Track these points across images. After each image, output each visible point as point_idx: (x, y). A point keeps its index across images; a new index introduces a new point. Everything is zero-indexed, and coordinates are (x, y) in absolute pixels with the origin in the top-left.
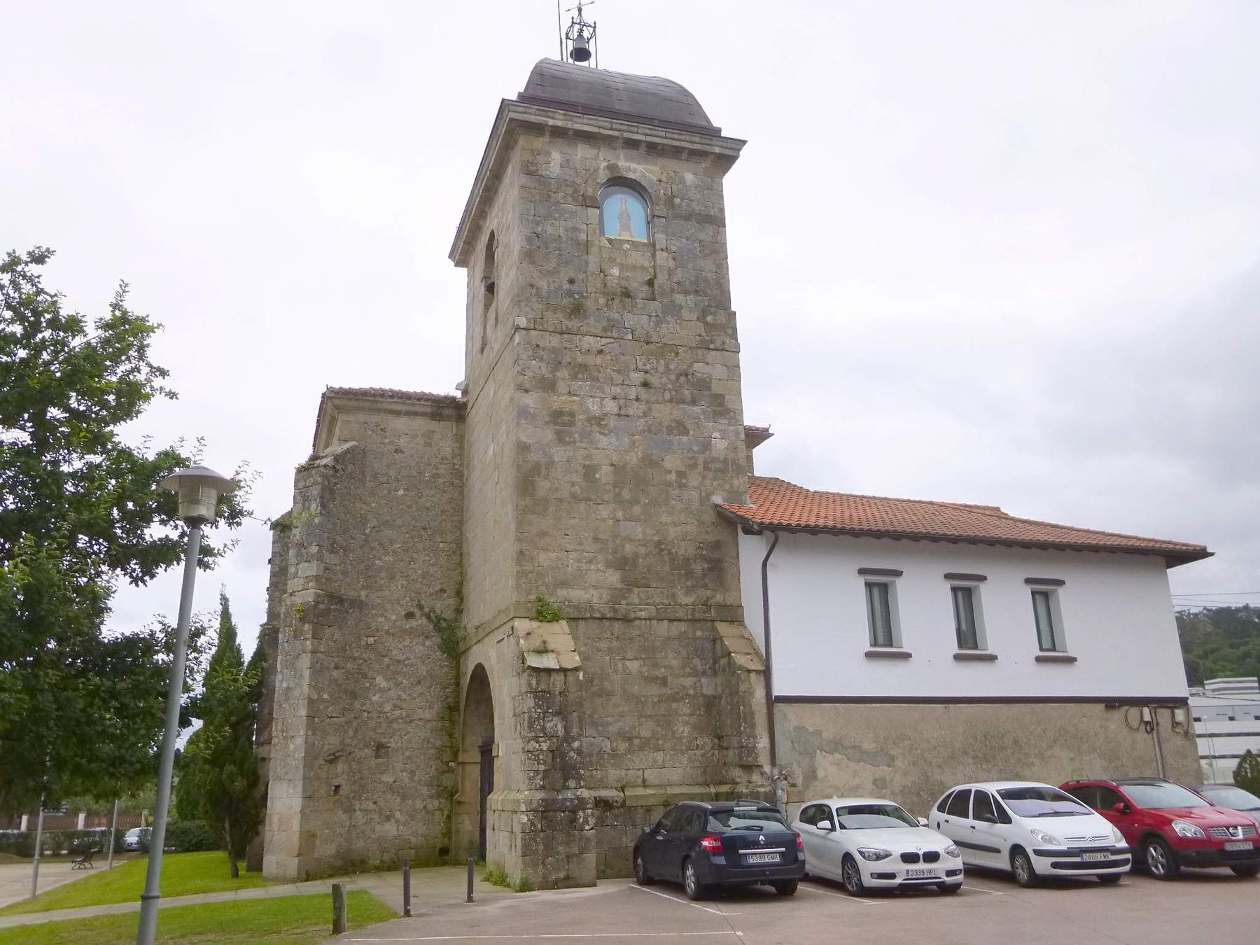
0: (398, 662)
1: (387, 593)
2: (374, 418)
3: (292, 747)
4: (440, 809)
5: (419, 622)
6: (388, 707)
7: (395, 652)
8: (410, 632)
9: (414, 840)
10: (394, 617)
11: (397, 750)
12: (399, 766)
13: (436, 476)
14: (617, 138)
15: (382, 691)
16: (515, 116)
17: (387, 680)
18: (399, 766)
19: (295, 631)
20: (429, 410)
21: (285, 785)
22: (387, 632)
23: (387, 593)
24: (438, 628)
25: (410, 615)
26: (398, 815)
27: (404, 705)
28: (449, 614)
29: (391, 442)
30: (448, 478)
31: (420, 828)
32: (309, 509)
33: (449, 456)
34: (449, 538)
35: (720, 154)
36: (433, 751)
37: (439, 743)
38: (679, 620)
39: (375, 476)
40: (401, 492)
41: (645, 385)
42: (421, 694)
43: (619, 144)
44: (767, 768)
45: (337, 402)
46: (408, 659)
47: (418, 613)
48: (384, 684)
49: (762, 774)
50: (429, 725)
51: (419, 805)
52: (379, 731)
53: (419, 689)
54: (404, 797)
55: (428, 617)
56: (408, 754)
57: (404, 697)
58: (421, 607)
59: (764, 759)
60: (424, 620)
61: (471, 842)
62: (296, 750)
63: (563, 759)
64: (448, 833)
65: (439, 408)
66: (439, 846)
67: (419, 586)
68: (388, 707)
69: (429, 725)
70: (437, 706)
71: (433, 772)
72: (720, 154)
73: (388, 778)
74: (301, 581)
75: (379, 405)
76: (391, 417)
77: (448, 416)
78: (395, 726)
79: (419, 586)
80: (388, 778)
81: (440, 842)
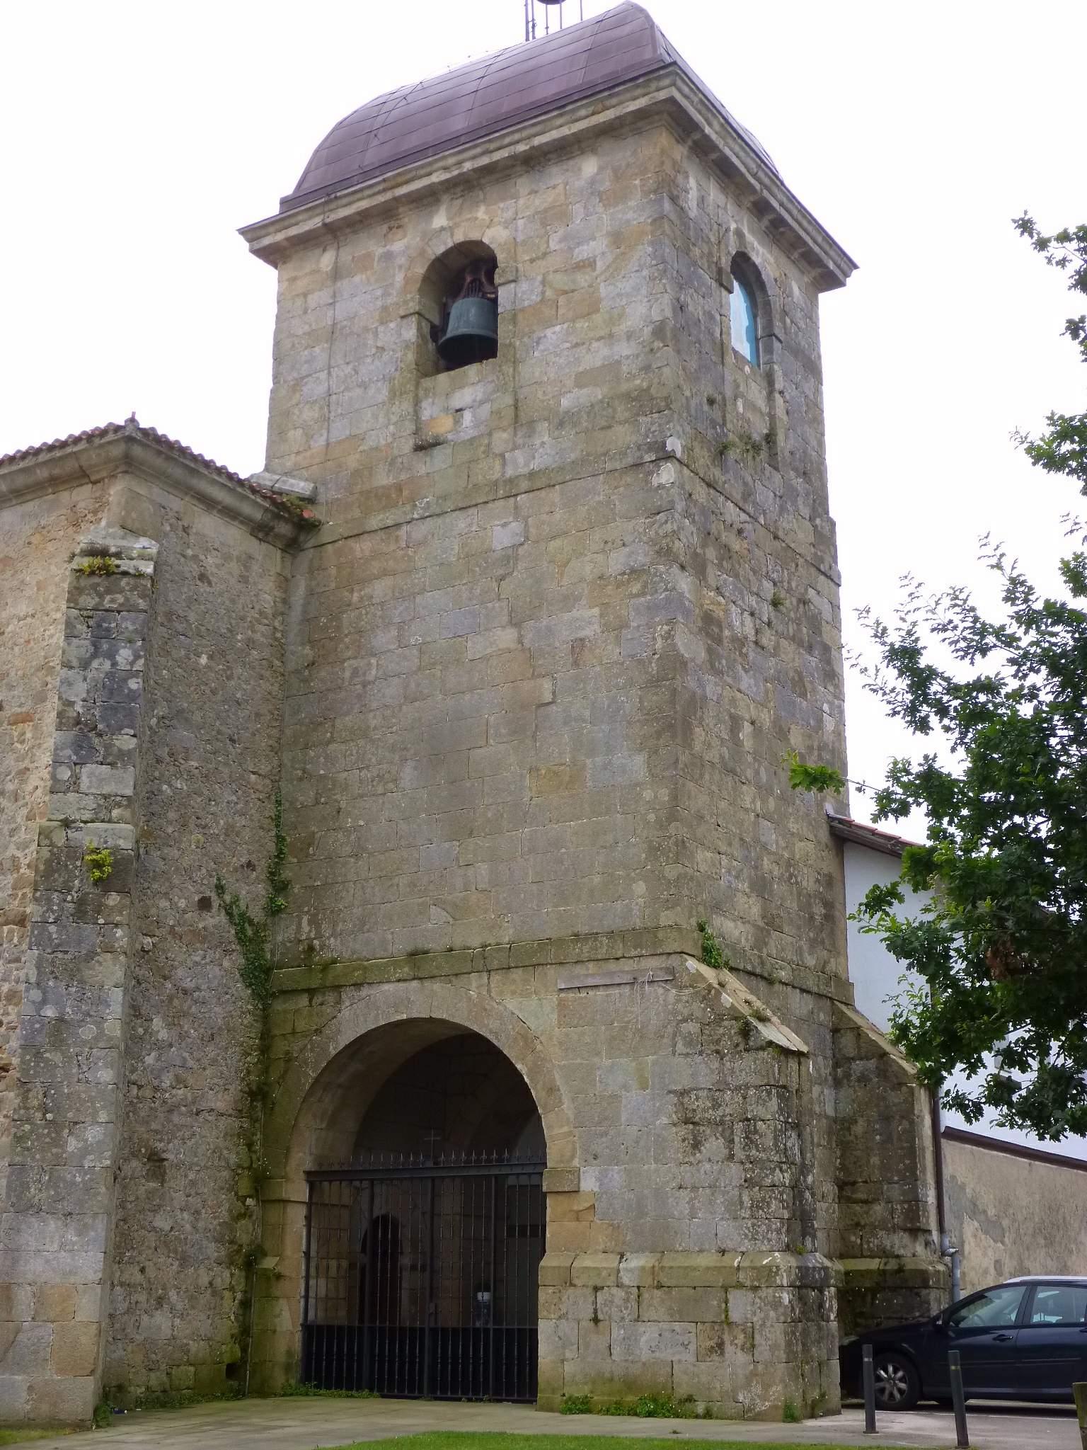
0: (185, 992)
1: (176, 853)
2: (176, 503)
3: (72, 1145)
4: (232, 1289)
5: (215, 919)
6: (167, 1081)
7: (180, 972)
8: (201, 936)
9: (194, 1347)
10: (182, 904)
11: (178, 1167)
12: (179, 1198)
13: (250, 643)
14: (754, 191)
15: (161, 1047)
16: (678, 96)
17: (170, 1025)
18: (179, 1198)
19: (81, 903)
20: (258, 515)
21: (52, 1225)
22: (172, 930)
23: (176, 853)
24: (241, 938)
25: (204, 904)
26: (173, 1295)
27: (191, 1081)
28: (257, 914)
29: (195, 557)
30: (266, 654)
31: (201, 1322)
32: (111, 655)
33: (269, 611)
34: (264, 768)
35: (825, 266)
36: (225, 1174)
37: (233, 1159)
38: (808, 992)
39: (169, 615)
40: (204, 660)
41: (776, 603)
42: (214, 1062)
43: (748, 200)
44: (935, 1236)
45: (137, 451)
46: (198, 989)
47: (216, 903)
48: (163, 1035)
49: (927, 1244)
50: (223, 1123)
51: (204, 1280)
52: (154, 1126)
53: (211, 1051)
54: (184, 1261)
55: (230, 914)
56: (191, 1176)
57: (191, 1063)
58: (220, 889)
59: (933, 1225)
60: (223, 918)
61: (289, 1353)
62: (85, 1151)
63: (801, 1202)
64: (244, 1333)
65: (277, 517)
66: (227, 1359)
67: (219, 849)
68: (167, 1081)
69: (223, 1123)
70: (235, 1088)
71: (224, 1215)
72: (825, 266)
73: (162, 1222)
74: (90, 803)
75: (195, 482)
76: (198, 509)
77: (277, 536)
78: (176, 1119)
79: (219, 849)
80: (162, 1222)
81: (230, 1352)
